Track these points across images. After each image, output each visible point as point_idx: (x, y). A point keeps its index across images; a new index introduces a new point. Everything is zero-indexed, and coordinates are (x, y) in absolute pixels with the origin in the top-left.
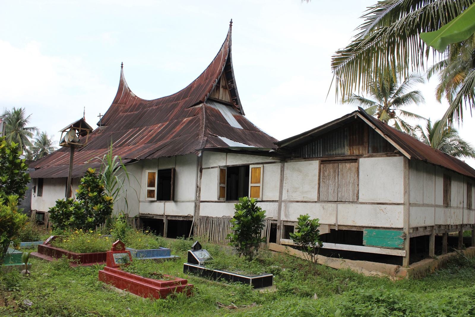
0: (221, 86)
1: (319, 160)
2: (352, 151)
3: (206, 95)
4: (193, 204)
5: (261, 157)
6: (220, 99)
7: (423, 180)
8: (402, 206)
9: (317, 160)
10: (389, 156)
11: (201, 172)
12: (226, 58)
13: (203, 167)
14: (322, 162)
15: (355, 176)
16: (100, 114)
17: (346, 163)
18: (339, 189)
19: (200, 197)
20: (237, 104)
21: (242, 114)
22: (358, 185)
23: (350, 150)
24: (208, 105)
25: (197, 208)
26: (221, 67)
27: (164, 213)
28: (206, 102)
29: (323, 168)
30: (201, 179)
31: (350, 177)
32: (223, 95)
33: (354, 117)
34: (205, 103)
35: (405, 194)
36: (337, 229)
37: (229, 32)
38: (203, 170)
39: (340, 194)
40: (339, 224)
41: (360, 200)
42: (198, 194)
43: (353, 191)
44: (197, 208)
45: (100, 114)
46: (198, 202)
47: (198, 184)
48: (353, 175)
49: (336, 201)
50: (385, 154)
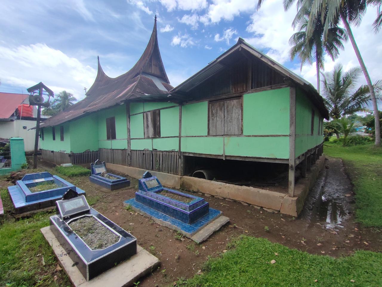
0: (153, 64)
1: (208, 100)
2: (236, 89)
3: (141, 69)
4: (126, 141)
5: (165, 103)
6: (153, 72)
7: (366, 103)
8: (288, 138)
9: (207, 100)
10: (274, 89)
11: (129, 118)
12: (154, 44)
13: (131, 114)
14: (210, 102)
15: (239, 112)
16: (85, 88)
17: (233, 100)
18: (225, 124)
19: (130, 136)
20: (165, 77)
21: (168, 83)
22: (242, 120)
23: (235, 88)
24: (144, 76)
25: (129, 143)
26: (151, 50)
27: (152, 140)
28: (142, 74)
29: (212, 107)
30: (129, 123)
31: (235, 113)
32: (154, 70)
33: (239, 50)
34: (141, 75)
35: (291, 126)
36: (224, 159)
37: (154, 25)
38: (131, 117)
39: (226, 129)
40: (226, 154)
41: (244, 133)
42: (129, 133)
43: (238, 126)
44: (129, 143)
45: (85, 88)
46: (129, 140)
47: (128, 126)
48: (238, 111)
49: (223, 135)
50: (270, 87)
